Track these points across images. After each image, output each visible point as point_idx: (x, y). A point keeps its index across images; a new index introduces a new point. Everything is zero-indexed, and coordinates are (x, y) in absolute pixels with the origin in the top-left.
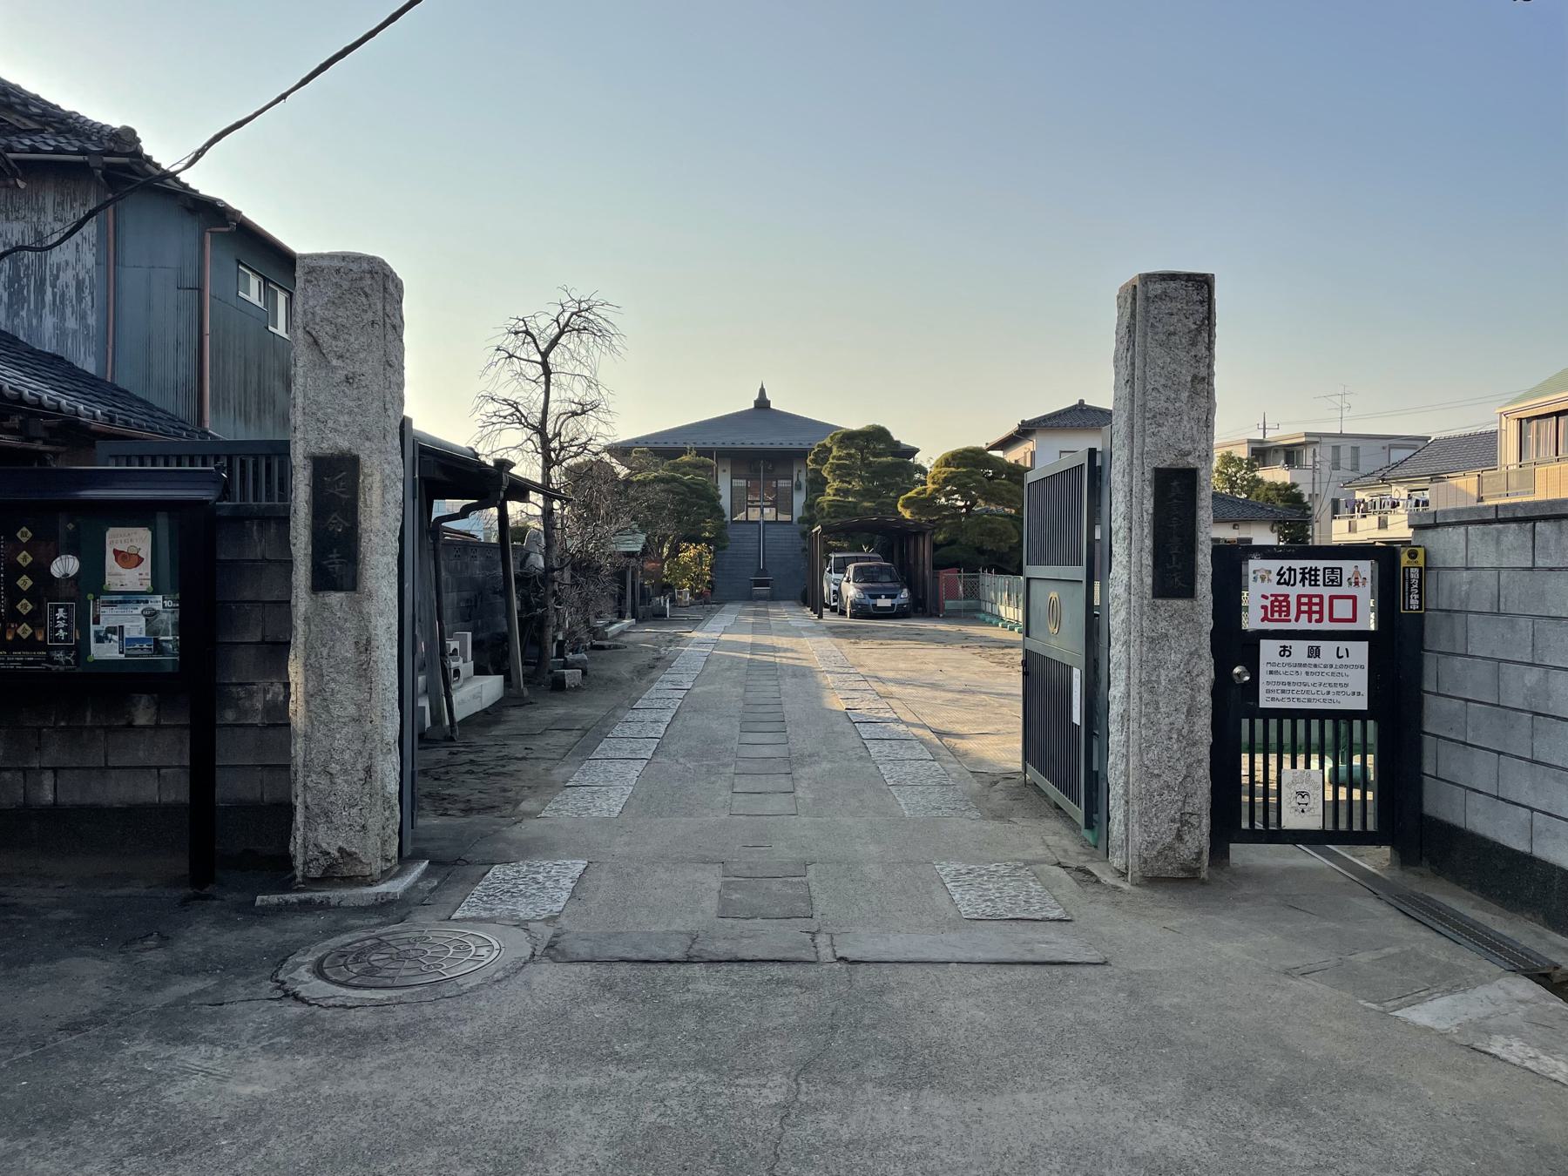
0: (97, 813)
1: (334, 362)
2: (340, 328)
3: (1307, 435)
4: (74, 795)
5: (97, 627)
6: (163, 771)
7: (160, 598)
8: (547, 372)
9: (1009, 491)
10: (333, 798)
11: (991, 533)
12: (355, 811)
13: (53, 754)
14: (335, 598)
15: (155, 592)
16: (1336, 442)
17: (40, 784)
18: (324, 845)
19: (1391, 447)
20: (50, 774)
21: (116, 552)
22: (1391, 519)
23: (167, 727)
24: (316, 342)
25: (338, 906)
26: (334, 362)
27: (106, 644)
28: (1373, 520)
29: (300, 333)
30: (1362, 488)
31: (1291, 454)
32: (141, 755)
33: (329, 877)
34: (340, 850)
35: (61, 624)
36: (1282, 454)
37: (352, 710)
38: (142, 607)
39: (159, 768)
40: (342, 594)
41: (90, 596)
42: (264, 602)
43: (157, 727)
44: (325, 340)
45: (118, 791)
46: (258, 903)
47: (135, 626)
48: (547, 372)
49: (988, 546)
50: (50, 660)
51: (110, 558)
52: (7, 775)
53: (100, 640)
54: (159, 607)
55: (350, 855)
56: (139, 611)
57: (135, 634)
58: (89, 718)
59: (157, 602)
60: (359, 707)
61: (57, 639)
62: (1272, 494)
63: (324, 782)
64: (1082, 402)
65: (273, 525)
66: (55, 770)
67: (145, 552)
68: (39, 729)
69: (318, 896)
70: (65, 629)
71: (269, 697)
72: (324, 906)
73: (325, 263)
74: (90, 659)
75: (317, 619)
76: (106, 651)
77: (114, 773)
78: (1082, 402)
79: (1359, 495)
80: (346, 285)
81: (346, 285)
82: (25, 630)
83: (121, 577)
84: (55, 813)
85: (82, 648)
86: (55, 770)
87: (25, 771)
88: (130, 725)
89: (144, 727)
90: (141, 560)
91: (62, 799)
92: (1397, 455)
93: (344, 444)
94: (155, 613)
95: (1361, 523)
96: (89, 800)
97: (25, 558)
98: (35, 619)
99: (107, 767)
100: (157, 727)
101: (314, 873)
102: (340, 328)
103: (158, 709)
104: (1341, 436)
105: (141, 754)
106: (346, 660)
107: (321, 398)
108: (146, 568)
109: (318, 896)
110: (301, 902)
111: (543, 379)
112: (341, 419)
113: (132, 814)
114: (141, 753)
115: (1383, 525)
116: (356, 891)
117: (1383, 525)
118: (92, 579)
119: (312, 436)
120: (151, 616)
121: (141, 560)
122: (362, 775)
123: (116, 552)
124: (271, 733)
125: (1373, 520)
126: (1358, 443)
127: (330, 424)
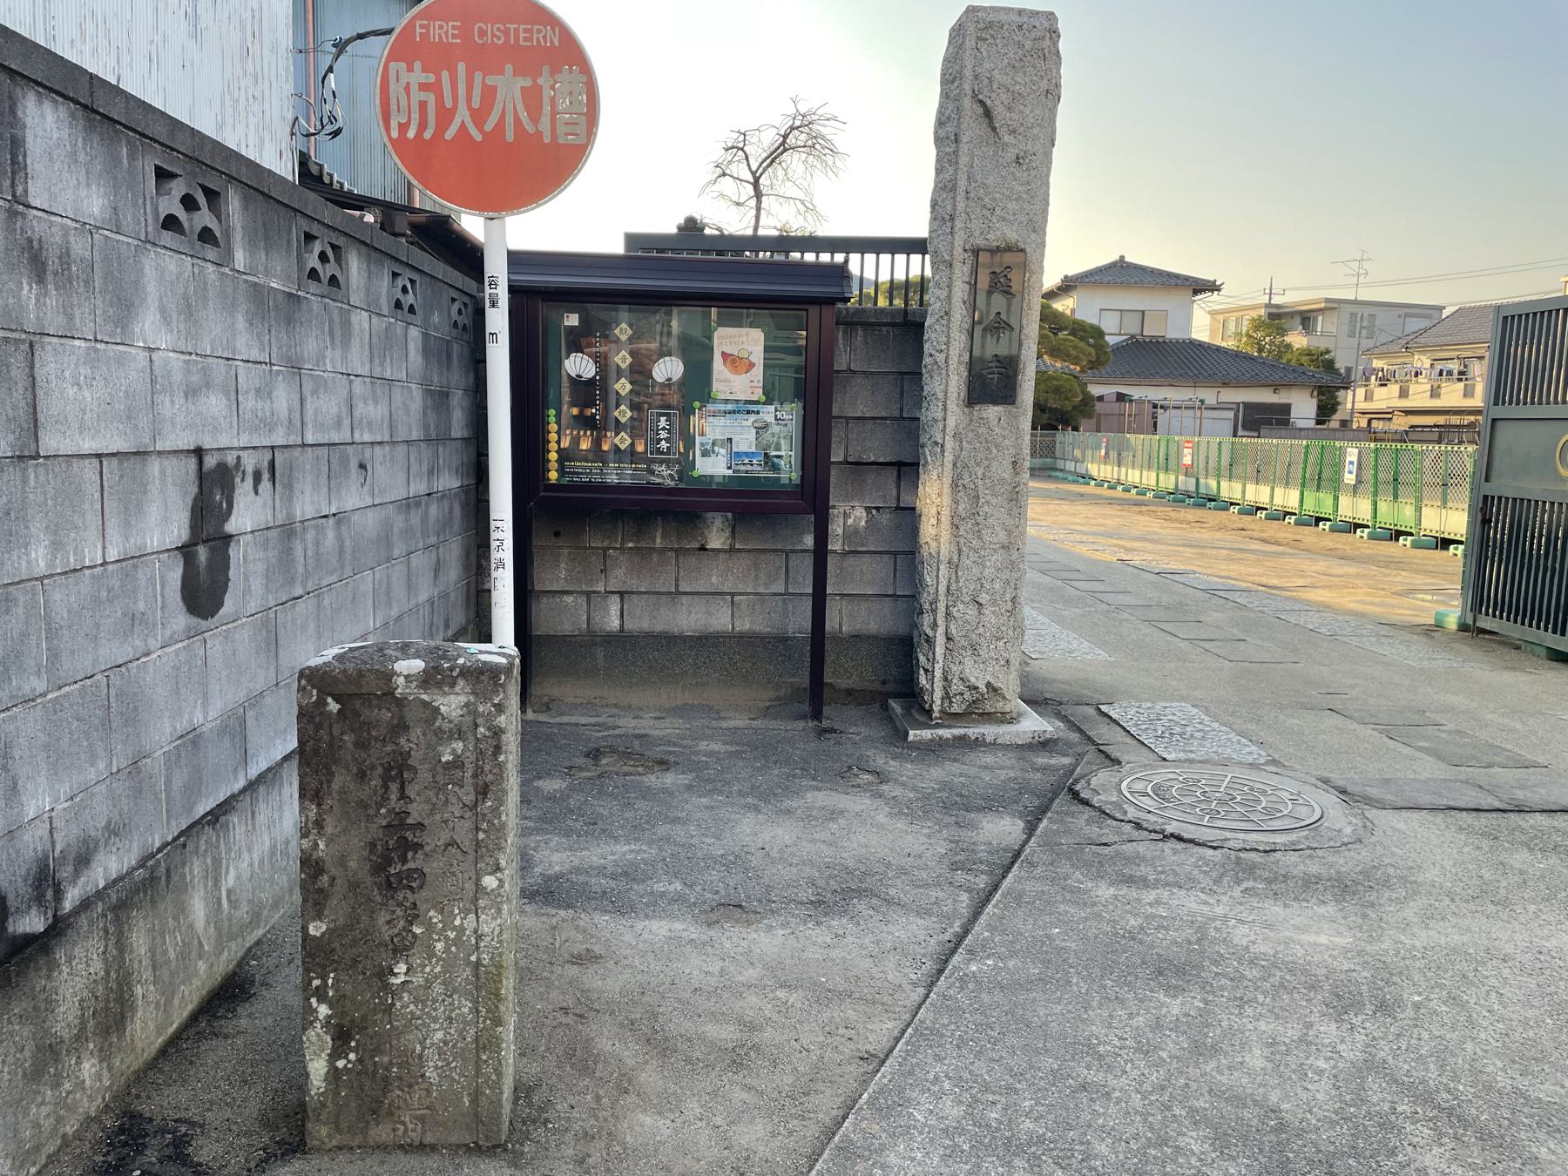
0: (668, 641)
1: (1007, 138)
2: (1017, 97)
3: (1327, 300)
4: (643, 620)
5: (704, 439)
6: (737, 598)
7: (771, 408)
8: (758, 195)
9: (1075, 347)
10: (981, 630)
11: (1057, 390)
12: (1001, 644)
13: (620, 577)
14: (993, 412)
15: (769, 402)
16: (1354, 309)
17: (606, 610)
18: (973, 680)
19: (1407, 315)
20: (616, 598)
21: (724, 354)
22: (1413, 388)
23: (740, 551)
24: (988, 114)
25: (994, 744)
26: (1007, 138)
27: (713, 458)
28: (1394, 389)
29: (967, 102)
30: (1381, 356)
31: (1306, 319)
32: (714, 581)
33: (977, 711)
34: (988, 685)
35: (663, 435)
36: (1298, 320)
37: (1002, 535)
38: (752, 418)
39: (733, 595)
40: (1000, 408)
41: (697, 404)
42: (848, 419)
43: (732, 550)
44: (999, 112)
45: (689, 619)
46: (910, 738)
47: (746, 441)
48: (758, 195)
49: (1052, 404)
50: (652, 472)
51: (718, 363)
52: (569, 599)
53: (705, 454)
54: (770, 419)
55: (995, 690)
56: (749, 423)
57: (743, 448)
58: (658, 540)
59: (768, 413)
60: (1009, 532)
61: (659, 452)
62: (1304, 359)
63: (972, 612)
64: (1122, 258)
65: (860, 332)
66: (621, 594)
67: (758, 356)
68: (605, 550)
69: (973, 732)
70: (667, 440)
71: (850, 521)
72: (978, 744)
73: (1003, 18)
74: (695, 474)
75: (971, 435)
76: (713, 467)
77: (685, 599)
78: (1122, 258)
79: (1377, 364)
80: (1028, 45)
81: (1028, 45)
82: (623, 440)
83: (730, 383)
84: (621, 642)
85: (687, 464)
86: (621, 594)
87: (588, 594)
88: (703, 549)
89: (719, 551)
90: (752, 365)
91: (629, 626)
92: (1415, 325)
93: (1012, 236)
94: (766, 426)
95: (1380, 393)
96: (659, 627)
97: (624, 359)
98: (635, 428)
99: (679, 593)
100: (732, 550)
101: (956, 709)
102: (1017, 97)
103: (733, 532)
104: (1355, 302)
105: (714, 579)
106: (1002, 481)
107: (990, 181)
108: (758, 373)
109: (973, 732)
110: (956, 738)
111: (753, 202)
112: (1009, 205)
113: (705, 642)
114: (714, 578)
115: (1404, 394)
116: (1005, 728)
117: (1404, 394)
118: (697, 386)
119: (976, 226)
120: (762, 428)
121: (752, 365)
122: (1009, 606)
123: (724, 354)
124: (851, 560)
125: (1394, 389)
126: (1373, 310)
127: (998, 212)
